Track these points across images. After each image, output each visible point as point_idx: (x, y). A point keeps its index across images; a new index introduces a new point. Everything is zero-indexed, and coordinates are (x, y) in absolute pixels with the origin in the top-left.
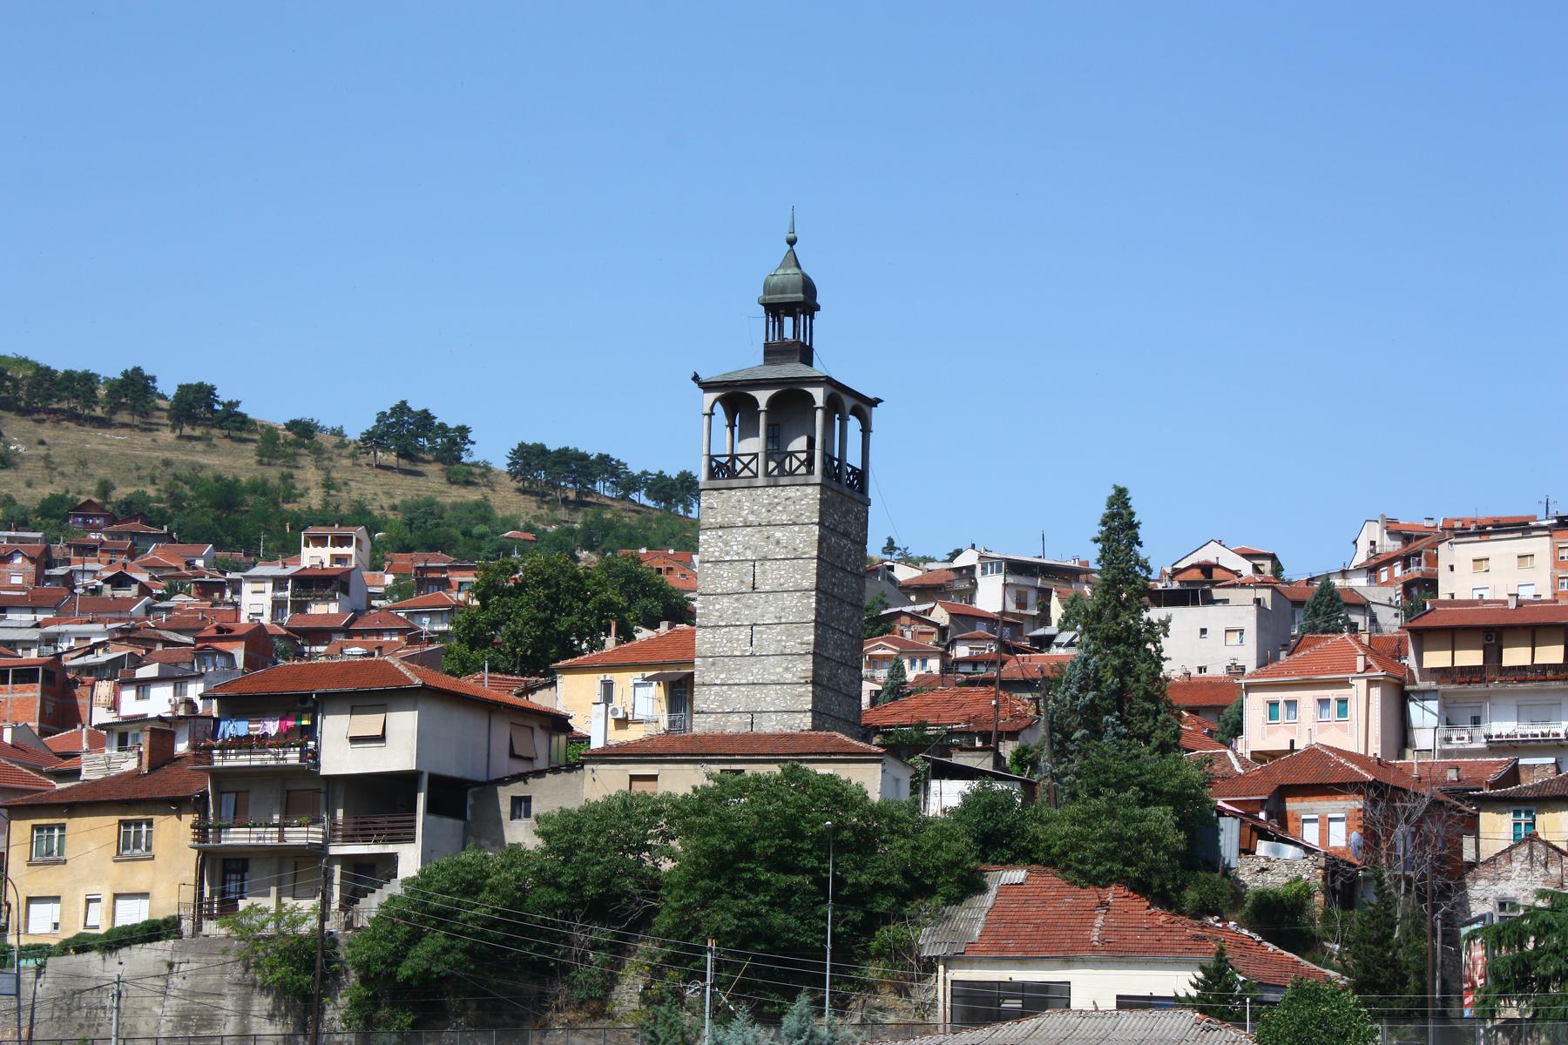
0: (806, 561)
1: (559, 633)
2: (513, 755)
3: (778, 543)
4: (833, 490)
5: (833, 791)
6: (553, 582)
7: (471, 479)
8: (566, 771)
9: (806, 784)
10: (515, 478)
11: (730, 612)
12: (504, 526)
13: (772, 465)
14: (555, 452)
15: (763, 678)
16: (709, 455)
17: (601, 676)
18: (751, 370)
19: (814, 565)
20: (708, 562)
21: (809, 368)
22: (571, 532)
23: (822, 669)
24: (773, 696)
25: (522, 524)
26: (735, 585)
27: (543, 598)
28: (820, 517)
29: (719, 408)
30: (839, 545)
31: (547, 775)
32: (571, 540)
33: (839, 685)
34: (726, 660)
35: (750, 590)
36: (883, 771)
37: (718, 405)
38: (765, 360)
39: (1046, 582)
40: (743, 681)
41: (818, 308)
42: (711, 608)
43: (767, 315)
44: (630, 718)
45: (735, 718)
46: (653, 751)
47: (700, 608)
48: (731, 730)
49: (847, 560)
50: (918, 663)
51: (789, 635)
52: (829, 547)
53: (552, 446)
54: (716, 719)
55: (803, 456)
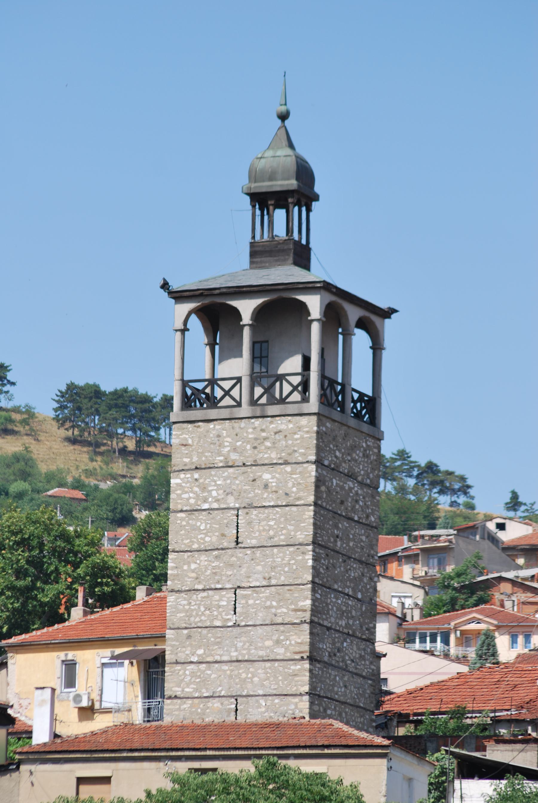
0: (301, 508)
1: (42, 605)
3: (266, 486)
4: (334, 421)
5: (319, 793)
6: (35, 543)
7: (10, 427)
9: (286, 785)
10: (63, 425)
11: (209, 572)
12: (48, 482)
13: (258, 391)
14: (110, 393)
15: (249, 654)
16: (182, 380)
17: (62, 655)
18: (233, 275)
19: (310, 512)
20: (182, 511)
21: (303, 272)
22: (128, 489)
24: (263, 676)
25: (70, 480)
26: (214, 539)
27: (23, 562)
28: (318, 454)
29: (195, 323)
30: (342, 488)
32: (128, 498)
33: (344, 661)
34: (205, 631)
35: (233, 544)
36: (390, 769)
38: (251, 263)
40: (225, 658)
41: (316, 198)
42: (185, 567)
43: (254, 207)
44: (97, 706)
45: (216, 704)
46: (105, 747)
49: (353, 507)
50: (521, 639)
53: (107, 387)
54: (192, 706)
55: (296, 380)
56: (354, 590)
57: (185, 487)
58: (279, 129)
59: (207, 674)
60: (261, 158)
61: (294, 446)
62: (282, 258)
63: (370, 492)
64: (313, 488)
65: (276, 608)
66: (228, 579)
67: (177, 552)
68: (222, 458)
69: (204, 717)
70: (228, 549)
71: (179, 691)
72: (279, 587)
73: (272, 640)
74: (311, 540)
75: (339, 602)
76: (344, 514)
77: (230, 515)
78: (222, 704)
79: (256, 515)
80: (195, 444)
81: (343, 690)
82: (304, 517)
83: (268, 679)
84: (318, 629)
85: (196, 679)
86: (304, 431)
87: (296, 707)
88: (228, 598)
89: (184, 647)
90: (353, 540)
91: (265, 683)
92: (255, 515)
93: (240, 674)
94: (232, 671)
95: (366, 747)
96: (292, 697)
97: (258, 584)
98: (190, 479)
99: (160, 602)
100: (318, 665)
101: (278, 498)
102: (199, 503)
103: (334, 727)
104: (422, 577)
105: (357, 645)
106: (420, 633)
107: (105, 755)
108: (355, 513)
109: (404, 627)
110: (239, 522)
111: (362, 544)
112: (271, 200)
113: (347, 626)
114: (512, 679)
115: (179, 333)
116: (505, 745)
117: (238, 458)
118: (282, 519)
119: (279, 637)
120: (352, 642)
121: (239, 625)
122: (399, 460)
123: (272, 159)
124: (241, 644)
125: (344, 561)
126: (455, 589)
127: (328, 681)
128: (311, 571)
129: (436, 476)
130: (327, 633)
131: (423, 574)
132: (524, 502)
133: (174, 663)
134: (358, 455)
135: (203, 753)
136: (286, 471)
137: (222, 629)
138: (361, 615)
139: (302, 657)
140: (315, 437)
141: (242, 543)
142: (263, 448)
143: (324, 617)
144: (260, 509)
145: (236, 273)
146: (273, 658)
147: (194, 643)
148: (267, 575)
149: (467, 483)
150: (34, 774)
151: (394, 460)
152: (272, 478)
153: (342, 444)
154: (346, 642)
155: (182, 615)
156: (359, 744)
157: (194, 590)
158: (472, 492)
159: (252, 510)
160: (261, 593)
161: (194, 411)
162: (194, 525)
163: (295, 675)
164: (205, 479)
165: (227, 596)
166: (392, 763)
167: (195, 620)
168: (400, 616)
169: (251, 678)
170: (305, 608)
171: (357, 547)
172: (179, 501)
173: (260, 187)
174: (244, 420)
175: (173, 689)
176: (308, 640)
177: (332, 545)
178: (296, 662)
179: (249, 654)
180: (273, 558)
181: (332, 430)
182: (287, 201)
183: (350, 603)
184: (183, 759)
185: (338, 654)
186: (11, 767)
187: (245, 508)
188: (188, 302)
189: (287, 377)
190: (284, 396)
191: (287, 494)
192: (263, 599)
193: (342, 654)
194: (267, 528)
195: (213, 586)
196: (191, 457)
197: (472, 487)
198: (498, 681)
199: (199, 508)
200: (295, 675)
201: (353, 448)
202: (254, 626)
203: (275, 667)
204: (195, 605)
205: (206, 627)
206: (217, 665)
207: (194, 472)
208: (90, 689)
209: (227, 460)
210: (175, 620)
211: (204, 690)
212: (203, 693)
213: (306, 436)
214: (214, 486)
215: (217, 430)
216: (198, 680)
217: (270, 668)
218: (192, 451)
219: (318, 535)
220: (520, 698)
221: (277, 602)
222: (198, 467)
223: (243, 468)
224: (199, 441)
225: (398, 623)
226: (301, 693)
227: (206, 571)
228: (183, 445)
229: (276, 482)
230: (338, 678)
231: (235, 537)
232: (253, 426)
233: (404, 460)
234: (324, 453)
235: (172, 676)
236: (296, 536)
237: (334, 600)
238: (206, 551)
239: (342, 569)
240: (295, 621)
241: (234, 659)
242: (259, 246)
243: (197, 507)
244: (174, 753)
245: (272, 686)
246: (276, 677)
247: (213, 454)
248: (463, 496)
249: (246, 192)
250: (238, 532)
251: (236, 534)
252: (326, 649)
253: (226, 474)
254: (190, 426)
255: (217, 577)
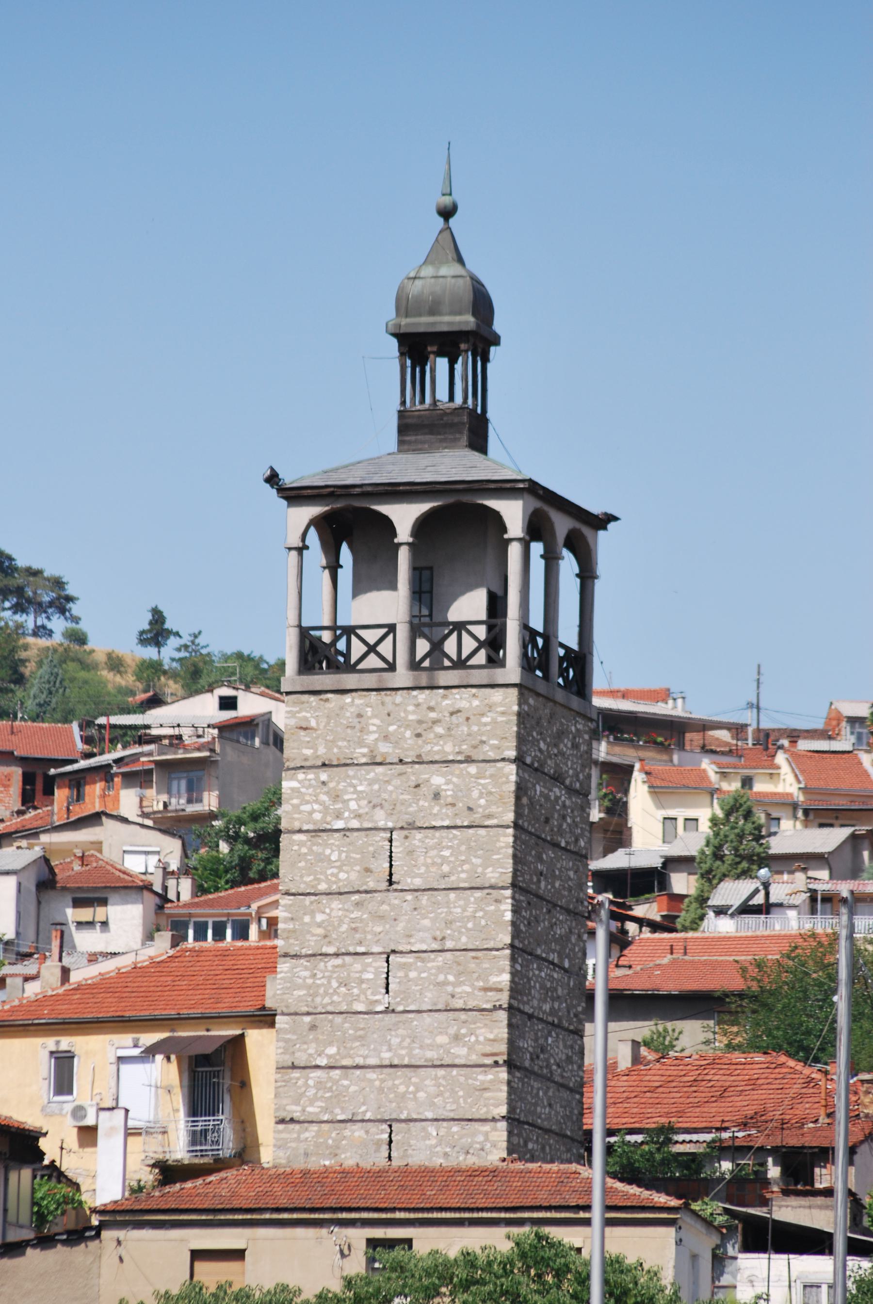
0: (493, 831)
3: (437, 796)
4: (538, 695)
8: (65, 1243)
11: (344, 927)
13: (423, 646)
16: (300, 626)
17: (50, 1043)
19: (507, 837)
20: (300, 831)
23: (522, 1036)
24: (432, 1090)
26: (353, 876)
28: (518, 748)
29: (313, 537)
30: (547, 798)
33: (548, 1066)
34: (338, 1019)
35: (384, 885)
36: (679, 1242)
37: (313, 531)
38: (401, 442)
39: (617, 749)
40: (372, 1061)
42: (307, 919)
45: (357, 1132)
46: (236, 1204)
48: (349, 1159)
52: (532, 804)
54: (318, 1134)
56: (560, 956)
57: (305, 794)
58: (441, 232)
59: (343, 1086)
60: (415, 278)
61: (481, 735)
63: (579, 801)
64: (512, 800)
65: (454, 985)
67: (294, 895)
68: (365, 750)
69: (338, 1152)
70: (375, 891)
71: (297, 1112)
72: (458, 953)
73: (447, 1034)
74: (509, 880)
75: (543, 974)
76: (549, 838)
77: (378, 839)
78: (367, 1132)
79: (420, 840)
80: (321, 727)
81: (547, 1110)
82: (498, 845)
83: (440, 1094)
84: (518, 1017)
85: (325, 1093)
86: (497, 712)
87: (487, 1140)
88: (376, 968)
89: (305, 1043)
91: (436, 1100)
92: (420, 840)
93: (397, 1087)
94: (383, 1081)
95: (643, 1209)
96: (480, 1123)
98: (313, 782)
99: (195, 958)
100: (518, 1074)
101: (456, 814)
102: (329, 819)
103: (582, 1176)
105: (563, 1040)
106: (195, 923)
107: (236, 1217)
108: (561, 835)
110: (393, 850)
111: (570, 883)
112: (432, 345)
113: (553, 1012)
114: (716, 1078)
115: (294, 553)
116: (798, 1198)
117: (391, 750)
118: (463, 848)
119: (459, 1030)
120: (557, 1037)
121: (393, 1011)
123: (433, 280)
124: (398, 1040)
125: (549, 911)
126: (247, 841)
127: (529, 1098)
128: (510, 928)
129: (9, 578)
132: (174, 630)
133: (288, 1068)
134: (566, 746)
135: (389, 1215)
136: (469, 773)
137: (366, 1016)
138: (568, 994)
139: (496, 1062)
140: (516, 722)
141: (398, 883)
142: (432, 735)
143: (525, 999)
144: (427, 831)
145: (378, 458)
146: (450, 1063)
147: (321, 1037)
148: (438, 934)
149: (67, 593)
150: (123, 1244)
152: (447, 783)
153: (547, 731)
154: (551, 1036)
156: (634, 1204)
157: (320, 955)
158: (75, 609)
160: (429, 962)
161: (320, 676)
162: (320, 854)
163: (485, 1089)
164: (338, 783)
165: (375, 964)
166: (683, 1234)
167: (322, 1002)
168: (160, 891)
169: (414, 1093)
170: (500, 987)
171: (564, 888)
172: (296, 816)
174: (400, 692)
175: (288, 1108)
176: (506, 1036)
178: (487, 1069)
181: (536, 709)
183: (555, 975)
184: (359, 1224)
185: (542, 1056)
186: (87, 1234)
187: (402, 828)
188: (308, 505)
189: (470, 627)
190: (464, 656)
191: (470, 809)
192: (433, 971)
193: (546, 1056)
196: (315, 748)
197: (78, 599)
198: (695, 1080)
199: (329, 827)
200: (485, 1089)
201: (561, 734)
202: (419, 1012)
203: (452, 1077)
204: (323, 977)
206: (358, 1072)
207: (320, 770)
209: (374, 754)
210: (290, 1001)
211: (337, 1111)
212: (337, 1115)
213: (500, 719)
214: (353, 793)
215: (358, 706)
216: (328, 1095)
217: (444, 1077)
218: (317, 738)
219: (519, 873)
220: (737, 1109)
221: (455, 976)
222: (327, 763)
223: (400, 767)
224: (328, 723)
225: (157, 905)
226: (494, 1118)
227: (339, 925)
228: (301, 728)
229: (453, 790)
230: (541, 1093)
231: (387, 873)
232: (415, 702)
234: (525, 746)
235: (286, 1088)
236: (486, 874)
237: (537, 972)
238: (341, 894)
239: (546, 923)
241: (387, 1063)
243: (325, 825)
244: (344, 1215)
245: (448, 1105)
246: (453, 1092)
247: (351, 743)
248: (58, 615)
249: (393, 331)
250: (391, 866)
251: (388, 869)
252: (527, 1049)
253: (372, 775)
254: (312, 698)
255: (358, 936)
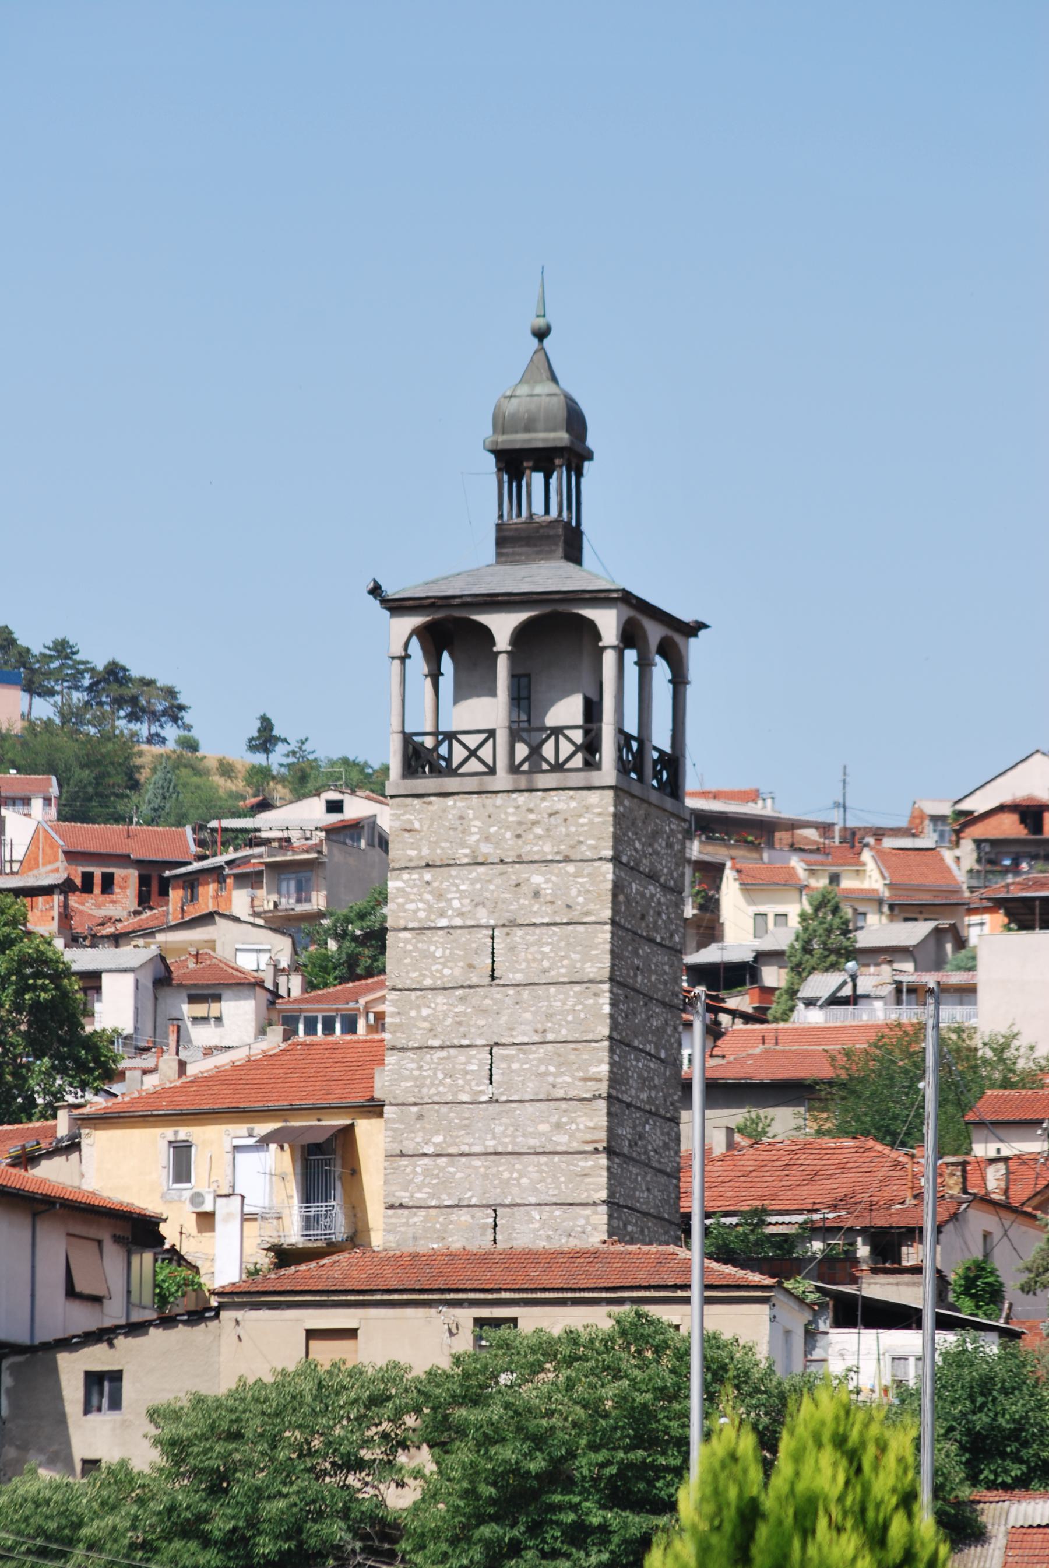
2: (71, 1292)
3: (537, 894)
4: (633, 796)
8: (185, 1323)
11: (449, 1021)
13: (522, 751)
15: (514, 1143)
16: (403, 732)
17: (170, 1133)
20: (405, 929)
23: (621, 1124)
26: (457, 972)
28: (615, 848)
30: (643, 895)
31: (152, 1330)
33: (646, 1153)
34: (444, 1109)
36: (773, 1319)
38: (499, 555)
39: (710, 848)
41: (589, 456)
42: (413, 1013)
45: (463, 1216)
46: (348, 1286)
47: (393, 1015)
48: (456, 1243)
51: (561, 1065)
52: (628, 901)
54: (426, 1219)
56: (657, 1048)
58: (535, 352)
60: (511, 397)
61: (579, 835)
62: (547, 549)
65: (555, 1075)
66: (480, 1032)
67: (400, 990)
68: (467, 851)
70: (478, 986)
75: (640, 1065)
76: (645, 934)
78: (473, 1217)
82: (597, 941)
87: (588, 1223)
88: (480, 1060)
89: (413, 1132)
90: (656, 972)
92: (520, 937)
94: (487, 1168)
97: (526, 1040)
98: (417, 882)
100: (617, 1160)
102: (433, 917)
104: (270, 911)
105: (661, 1127)
106: (305, 1017)
107: (349, 1298)
109: (278, 1006)
112: (528, 460)
113: (650, 1100)
114: (807, 1162)
115: (397, 662)
117: (492, 851)
118: (563, 944)
120: (655, 1124)
121: (497, 1101)
122: (57, 658)
123: (528, 399)
124: (502, 1129)
125: (646, 1004)
126: (355, 939)
127: (628, 1183)
128: (608, 1021)
130: (627, 1112)
131: (271, 906)
132: (282, 737)
134: (660, 845)
136: (567, 872)
138: (665, 1083)
139: (596, 1149)
140: (612, 822)
141: (500, 978)
142: (531, 836)
143: (623, 1088)
145: (478, 570)
147: (428, 1126)
149: (179, 702)
150: (242, 1323)
151: (46, 658)
155: (410, 1084)
158: (187, 717)
159: (515, 929)
164: (442, 882)
165: (479, 1056)
167: (429, 1092)
168: (271, 988)
172: (401, 914)
173: (511, 441)
174: (500, 795)
175: (397, 1194)
176: (605, 1124)
177: (631, 981)
179: (514, 1143)
180: (549, 1001)
181: (631, 810)
182: (554, 463)
183: (652, 1066)
184: (466, 1304)
185: (640, 1143)
186: (207, 1315)
187: (504, 925)
191: (569, 907)
192: (535, 1062)
194: (539, 957)
195: (456, 1042)
199: (433, 925)
201: (655, 834)
205: (447, 1103)
206: (464, 1159)
207: (424, 870)
208: (215, 1184)
211: (444, 1196)
213: (597, 820)
214: (456, 892)
216: (435, 1181)
217: (546, 1164)
218: (421, 839)
221: (555, 1066)
223: (501, 867)
224: (431, 825)
227: (444, 1019)
228: (406, 830)
230: (639, 1178)
231: (490, 969)
233: (67, 657)
238: (445, 989)
240: (585, 1096)
241: (491, 1150)
242: (510, 530)
244: (452, 1296)
246: (555, 1178)
250: (493, 962)
253: (474, 875)
254: (416, 801)
255: (462, 1029)
